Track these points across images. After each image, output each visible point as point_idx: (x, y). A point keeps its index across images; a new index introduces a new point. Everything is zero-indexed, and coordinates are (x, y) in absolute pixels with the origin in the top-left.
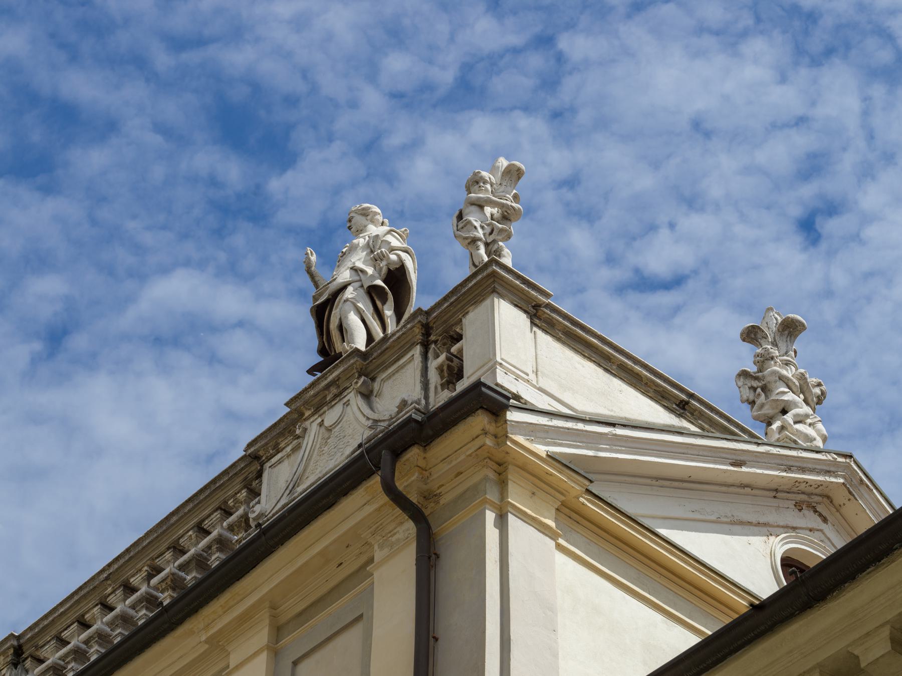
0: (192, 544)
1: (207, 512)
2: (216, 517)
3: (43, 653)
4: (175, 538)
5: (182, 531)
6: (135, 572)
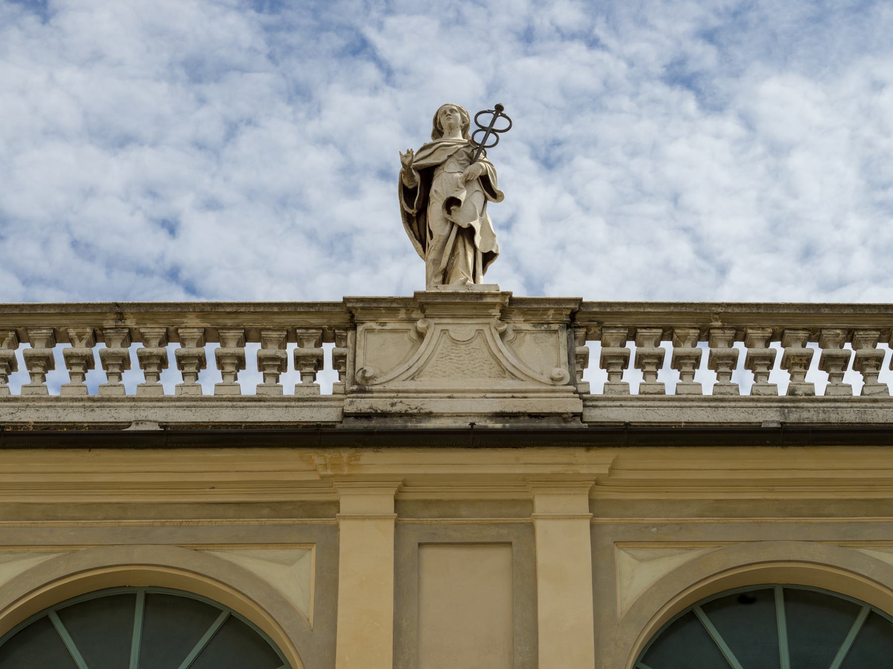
0: (834, 340)
1: (866, 326)
2: (874, 336)
3: (608, 334)
4: (819, 326)
5: (829, 325)
6: (757, 327)
